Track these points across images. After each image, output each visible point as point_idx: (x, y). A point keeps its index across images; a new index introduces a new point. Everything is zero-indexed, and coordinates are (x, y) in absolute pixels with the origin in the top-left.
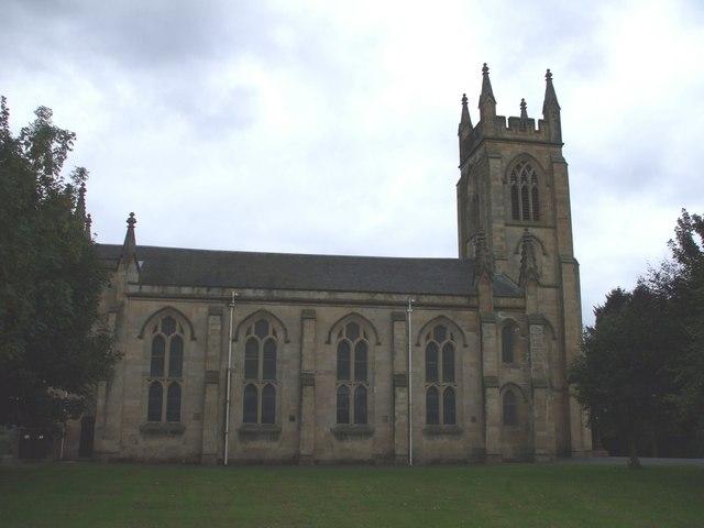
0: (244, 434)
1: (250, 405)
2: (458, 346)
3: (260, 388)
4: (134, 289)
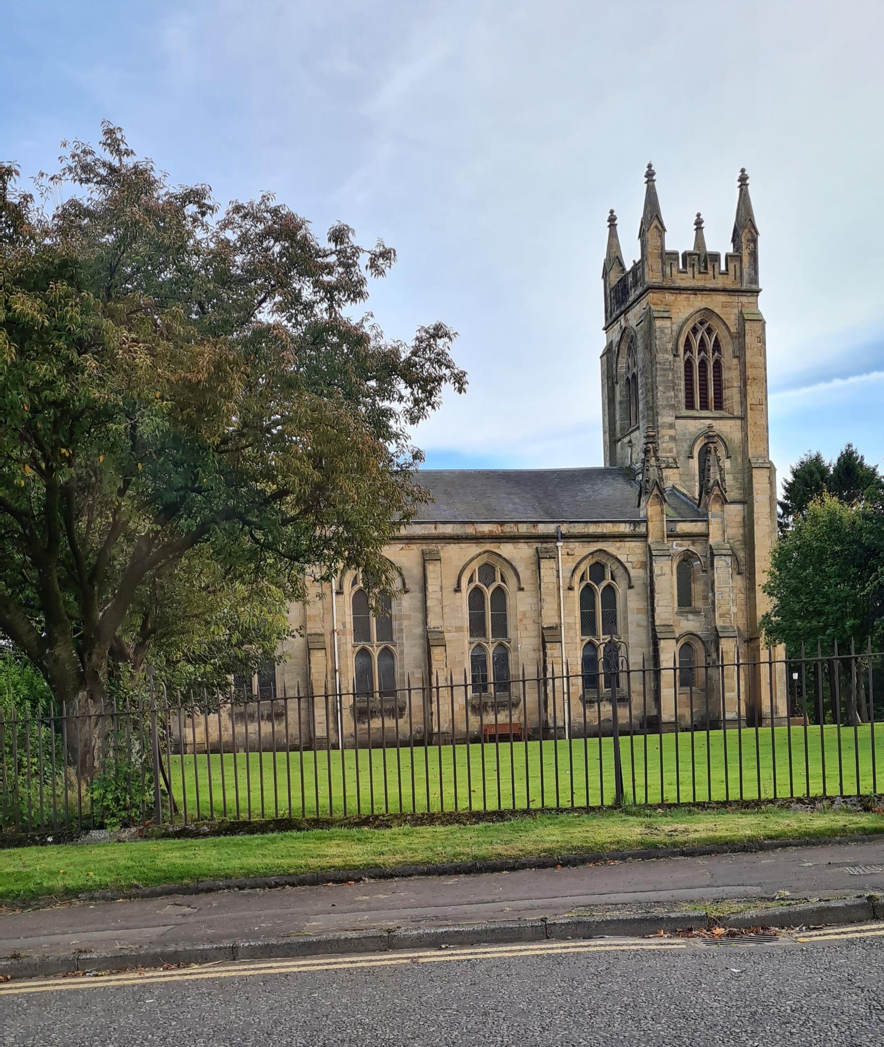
2: (620, 588)
3: (375, 653)
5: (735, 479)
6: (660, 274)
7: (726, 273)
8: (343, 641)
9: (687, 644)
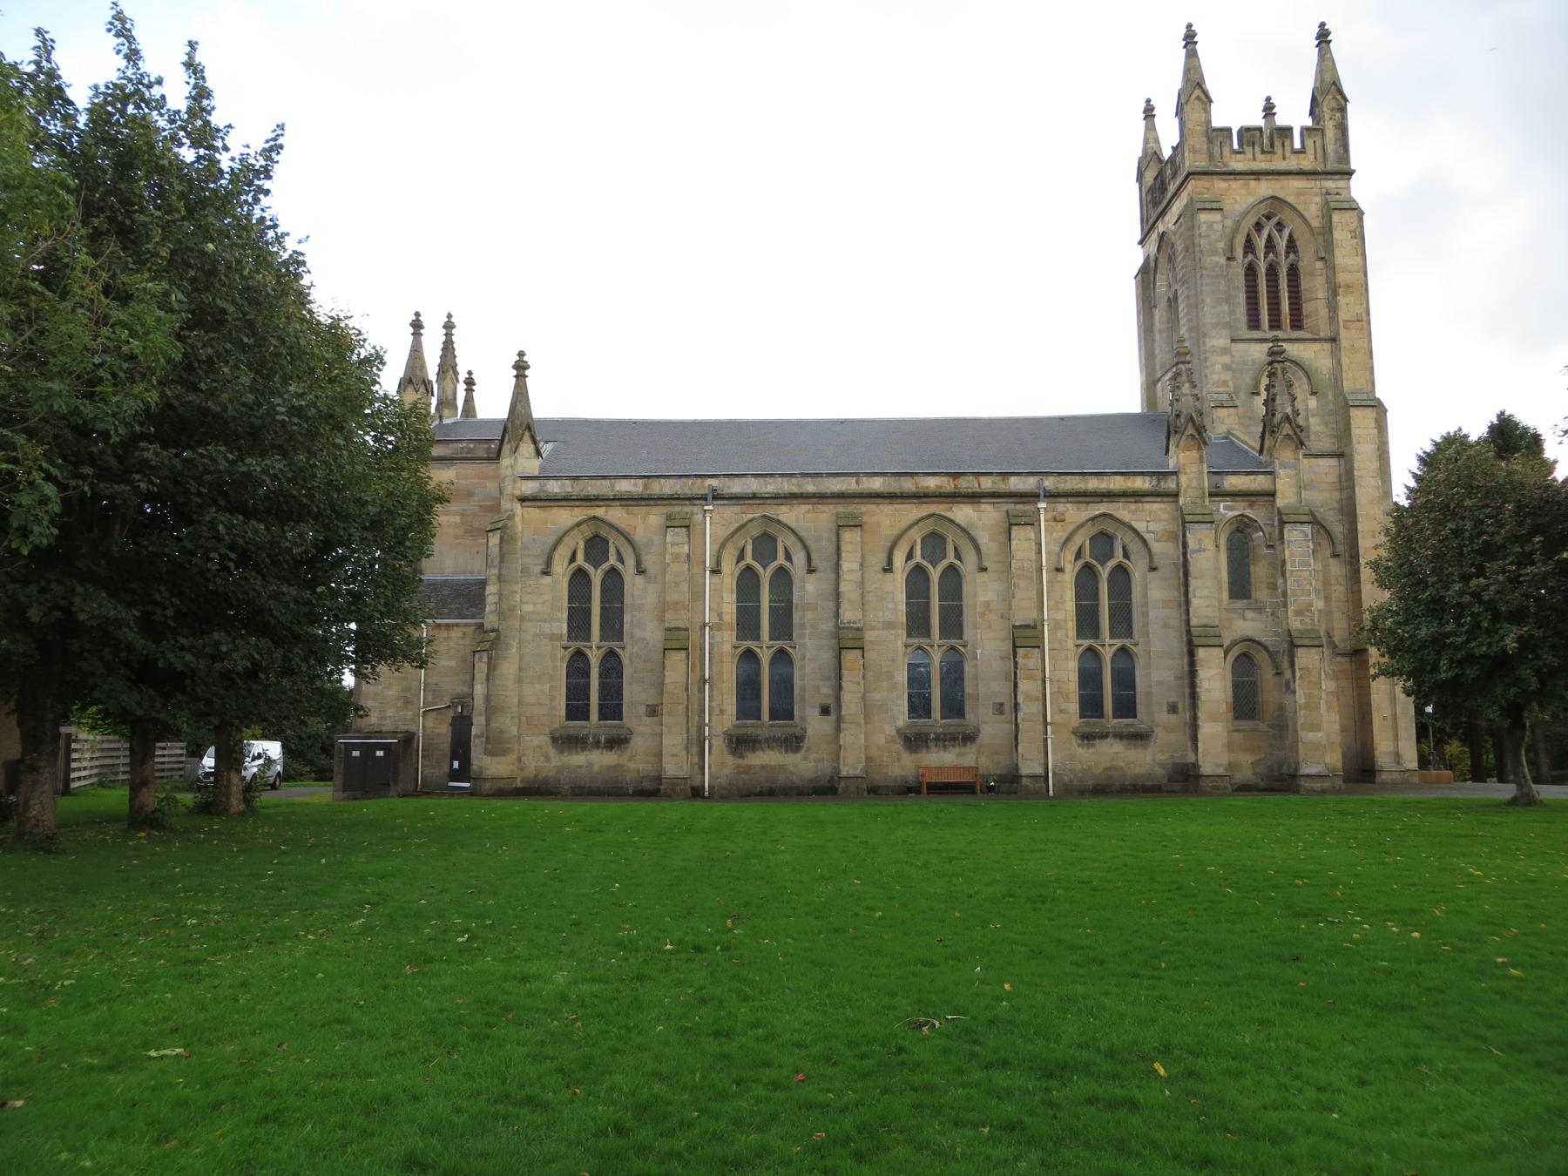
0: (740, 743)
1: (748, 689)
2: (1138, 570)
3: (765, 657)
4: (529, 488)
5: (1326, 424)
6: (1206, 156)
7: (1302, 151)
8: (718, 639)
9: (1245, 656)
